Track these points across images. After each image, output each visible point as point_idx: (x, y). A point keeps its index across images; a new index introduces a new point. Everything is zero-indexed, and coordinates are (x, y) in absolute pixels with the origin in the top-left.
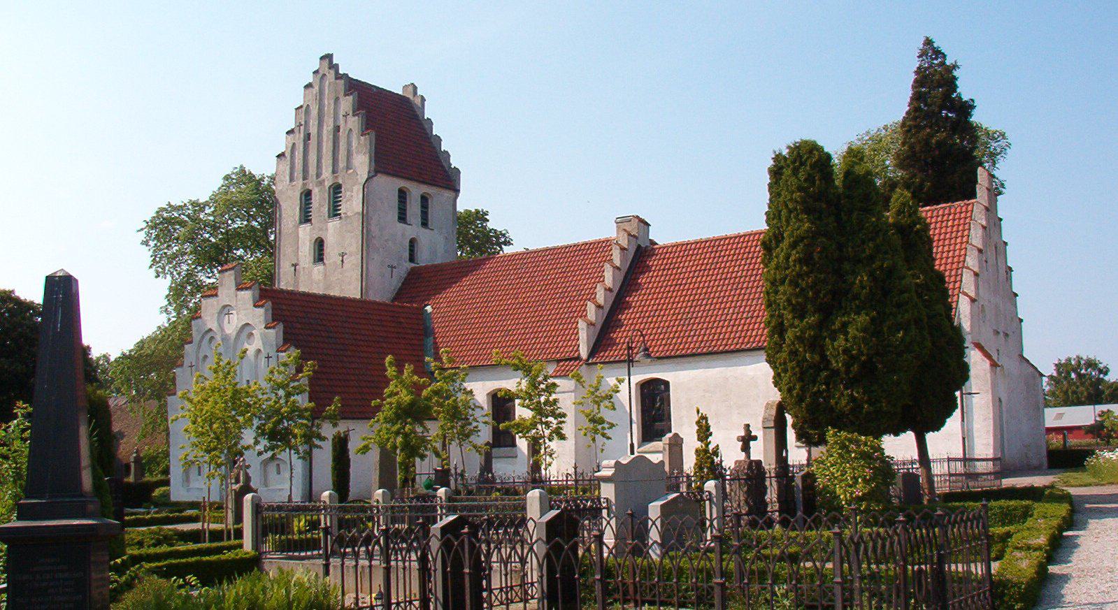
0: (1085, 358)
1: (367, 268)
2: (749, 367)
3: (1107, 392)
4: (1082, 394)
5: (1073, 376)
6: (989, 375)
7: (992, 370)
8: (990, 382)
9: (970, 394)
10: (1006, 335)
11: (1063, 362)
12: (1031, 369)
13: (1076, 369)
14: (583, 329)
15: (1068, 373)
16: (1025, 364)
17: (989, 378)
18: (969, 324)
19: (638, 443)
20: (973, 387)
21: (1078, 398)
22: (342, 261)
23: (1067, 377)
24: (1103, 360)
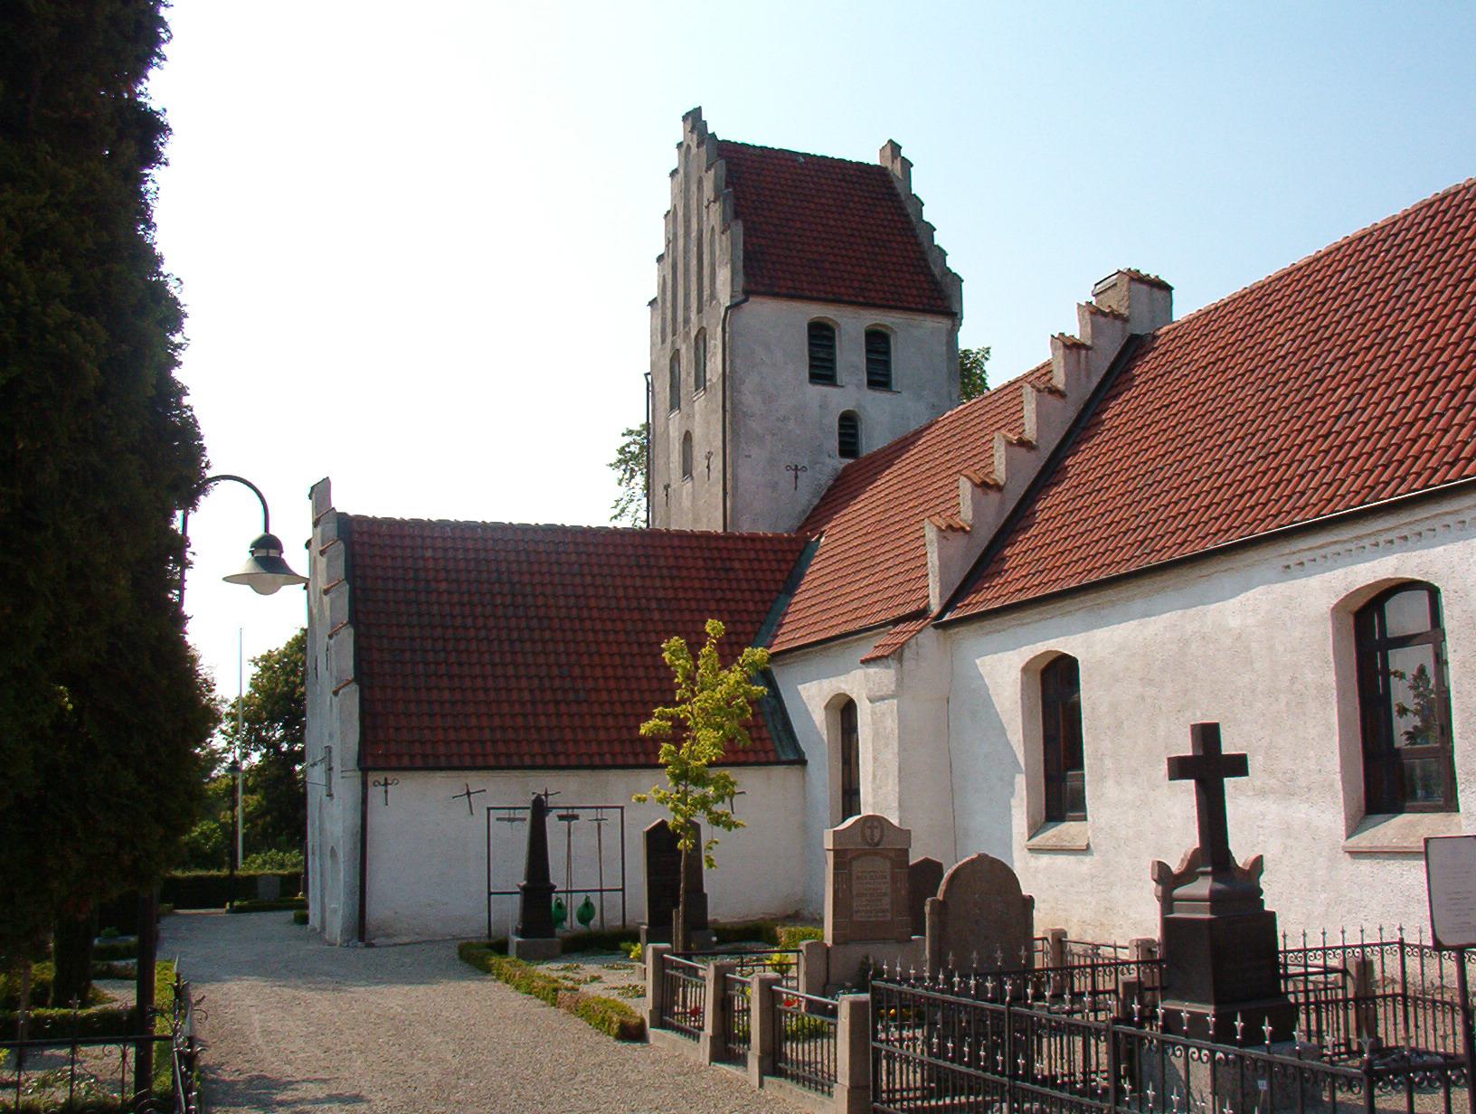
1: (734, 476)
2: (1233, 603)
14: (931, 541)
19: (1030, 816)
22: (708, 467)
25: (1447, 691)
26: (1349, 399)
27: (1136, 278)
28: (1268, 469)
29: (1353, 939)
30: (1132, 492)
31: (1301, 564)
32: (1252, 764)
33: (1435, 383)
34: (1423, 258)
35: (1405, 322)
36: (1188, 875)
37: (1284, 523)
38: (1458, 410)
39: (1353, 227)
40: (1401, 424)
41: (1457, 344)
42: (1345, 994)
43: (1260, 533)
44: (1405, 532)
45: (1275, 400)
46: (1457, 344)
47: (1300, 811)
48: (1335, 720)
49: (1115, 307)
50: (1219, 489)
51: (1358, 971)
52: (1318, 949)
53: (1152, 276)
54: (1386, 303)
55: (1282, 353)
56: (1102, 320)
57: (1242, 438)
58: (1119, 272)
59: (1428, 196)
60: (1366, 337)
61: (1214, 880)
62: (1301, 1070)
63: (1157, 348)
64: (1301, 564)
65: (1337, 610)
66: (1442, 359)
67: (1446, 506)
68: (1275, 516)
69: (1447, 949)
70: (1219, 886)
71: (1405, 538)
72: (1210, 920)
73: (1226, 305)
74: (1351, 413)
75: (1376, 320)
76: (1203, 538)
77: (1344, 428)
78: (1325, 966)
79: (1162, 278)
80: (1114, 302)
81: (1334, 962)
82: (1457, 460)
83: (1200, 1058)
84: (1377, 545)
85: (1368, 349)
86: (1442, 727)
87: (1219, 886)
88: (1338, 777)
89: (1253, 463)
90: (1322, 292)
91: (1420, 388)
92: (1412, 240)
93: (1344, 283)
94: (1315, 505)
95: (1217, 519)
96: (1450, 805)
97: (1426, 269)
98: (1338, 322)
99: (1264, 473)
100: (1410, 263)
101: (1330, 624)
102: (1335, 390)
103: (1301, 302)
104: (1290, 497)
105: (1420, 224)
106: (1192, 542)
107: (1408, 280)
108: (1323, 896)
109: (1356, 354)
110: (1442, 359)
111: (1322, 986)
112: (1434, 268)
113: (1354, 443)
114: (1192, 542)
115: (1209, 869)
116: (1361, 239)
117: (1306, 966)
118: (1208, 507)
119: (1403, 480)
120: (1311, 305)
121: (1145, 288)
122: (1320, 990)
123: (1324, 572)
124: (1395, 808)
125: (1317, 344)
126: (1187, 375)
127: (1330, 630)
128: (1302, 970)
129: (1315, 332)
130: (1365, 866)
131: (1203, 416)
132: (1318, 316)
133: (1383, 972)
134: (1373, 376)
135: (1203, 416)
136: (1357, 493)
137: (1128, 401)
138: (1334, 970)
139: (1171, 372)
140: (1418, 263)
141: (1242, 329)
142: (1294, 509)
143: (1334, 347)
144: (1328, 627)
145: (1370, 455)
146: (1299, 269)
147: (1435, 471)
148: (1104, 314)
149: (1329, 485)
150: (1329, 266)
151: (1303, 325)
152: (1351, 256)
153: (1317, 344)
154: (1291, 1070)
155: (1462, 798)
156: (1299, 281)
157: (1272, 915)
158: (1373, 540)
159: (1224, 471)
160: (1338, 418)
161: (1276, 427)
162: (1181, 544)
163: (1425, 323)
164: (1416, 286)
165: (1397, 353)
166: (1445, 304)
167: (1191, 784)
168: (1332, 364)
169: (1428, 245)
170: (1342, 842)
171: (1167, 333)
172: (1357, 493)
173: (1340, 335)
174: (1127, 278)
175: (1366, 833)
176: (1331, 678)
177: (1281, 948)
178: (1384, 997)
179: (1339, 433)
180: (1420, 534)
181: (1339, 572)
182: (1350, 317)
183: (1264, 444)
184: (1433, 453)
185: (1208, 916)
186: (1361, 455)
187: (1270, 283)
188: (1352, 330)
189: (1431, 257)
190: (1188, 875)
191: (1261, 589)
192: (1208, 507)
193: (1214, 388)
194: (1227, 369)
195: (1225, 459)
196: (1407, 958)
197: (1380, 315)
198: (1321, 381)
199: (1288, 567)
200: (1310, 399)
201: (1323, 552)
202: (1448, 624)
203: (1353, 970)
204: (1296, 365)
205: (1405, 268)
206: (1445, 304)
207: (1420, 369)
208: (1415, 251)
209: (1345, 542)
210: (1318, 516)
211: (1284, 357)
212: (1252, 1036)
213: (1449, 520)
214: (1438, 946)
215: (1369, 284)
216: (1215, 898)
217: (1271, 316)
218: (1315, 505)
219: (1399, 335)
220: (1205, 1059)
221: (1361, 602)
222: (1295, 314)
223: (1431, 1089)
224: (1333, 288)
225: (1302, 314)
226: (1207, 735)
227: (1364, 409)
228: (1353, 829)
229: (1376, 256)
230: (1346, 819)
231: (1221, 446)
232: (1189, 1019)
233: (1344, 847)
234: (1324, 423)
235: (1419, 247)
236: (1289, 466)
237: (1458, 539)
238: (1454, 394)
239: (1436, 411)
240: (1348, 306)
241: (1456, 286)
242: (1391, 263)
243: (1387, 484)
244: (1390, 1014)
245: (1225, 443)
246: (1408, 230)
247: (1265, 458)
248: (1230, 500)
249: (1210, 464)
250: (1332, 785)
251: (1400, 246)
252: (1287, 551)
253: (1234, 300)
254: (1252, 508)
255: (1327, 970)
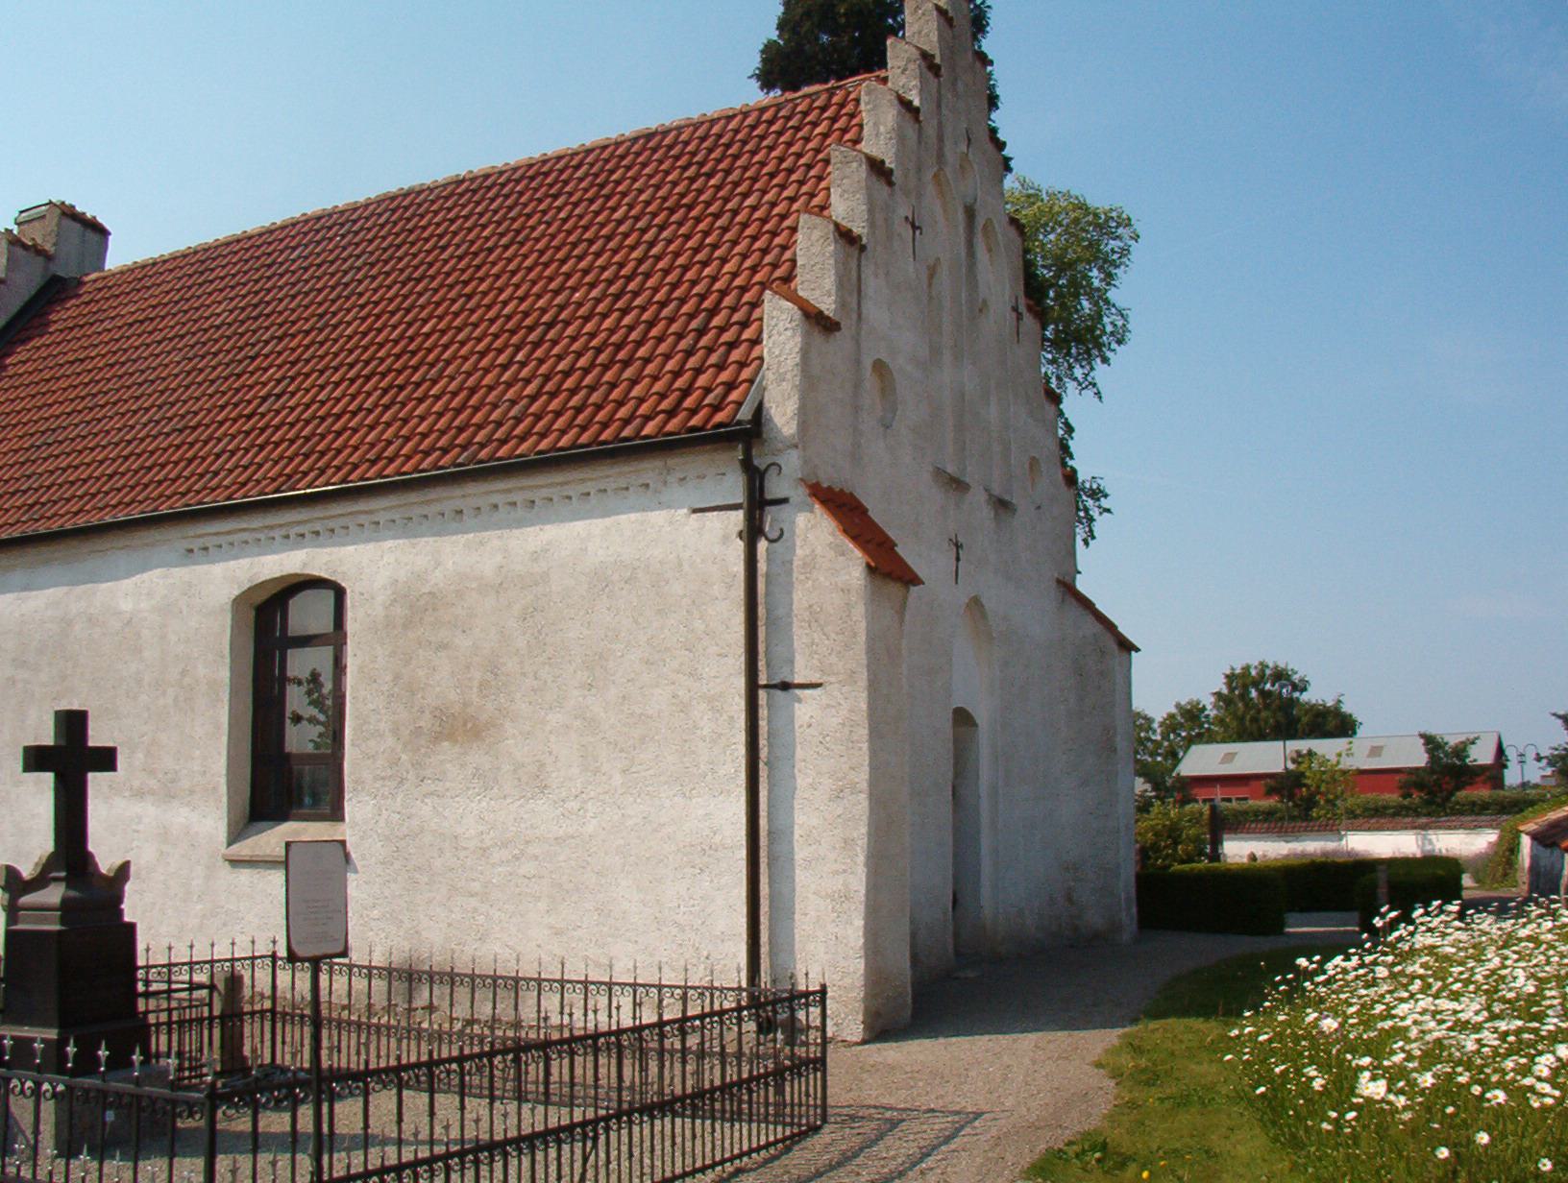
0: (1271, 665)
2: (127, 584)
3: (1305, 720)
4: (1266, 722)
5: (1254, 693)
6: (859, 611)
7: (874, 598)
8: (862, 638)
9: (786, 686)
10: (1002, 505)
11: (1238, 671)
12: (1092, 627)
13: (1256, 683)
15: (1245, 688)
16: (1074, 610)
17: (862, 627)
18: (792, 406)
20: (800, 662)
21: (1259, 729)
23: (1244, 696)
24: (1300, 669)
25: (343, 697)
26: (279, 381)
27: (69, 213)
28: (183, 443)
29: (222, 952)
30: (27, 449)
31: (206, 549)
32: (121, 761)
33: (368, 378)
34: (377, 249)
35: (349, 311)
36: (40, 881)
37: (192, 503)
38: (387, 408)
39: (312, 207)
40: (328, 415)
41: (396, 342)
42: (211, 1010)
43: (164, 510)
44: (318, 527)
45: (201, 371)
46: (396, 342)
47: (180, 816)
48: (225, 719)
49: (39, 241)
50: (127, 458)
51: (226, 985)
52: (183, 964)
53: (89, 215)
54: (333, 288)
55: (217, 323)
56: (20, 251)
57: (160, 407)
58: (50, 203)
59: (393, 189)
60: (307, 320)
61: (68, 887)
62: (139, 1097)
63: (81, 296)
64: (206, 549)
65: (239, 602)
66: (379, 355)
67: (362, 505)
68: (184, 495)
69: (303, 960)
70: (72, 893)
71: (317, 533)
72: (59, 932)
73: (165, 262)
74: (279, 396)
75: (320, 304)
76: (102, 509)
77: (269, 411)
78: (191, 982)
79: (100, 220)
80: (37, 235)
81: (201, 977)
82: (379, 458)
83: (22, 1091)
84: (287, 537)
85: (308, 333)
86: (335, 733)
87: (72, 893)
88: (223, 780)
89: (168, 435)
90: (269, 266)
91: (353, 381)
92: (369, 230)
93: (294, 261)
94: (227, 487)
95: (119, 490)
96: (336, 814)
97: (378, 261)
98: (281, 300)
99: (178, 447)
100: (363, 252)
101: (229, 617)
102: (266, 370)
103: (246, 273)
104: (202, 476)
105: (380, 215)
106: (89, 512)
107: (359, 269)
108: (199, 907)
109: (294, 336)
110: (379, 355)
111: (185, 1004)
112: (386, 262)
113: (278, 428)
114: (89, 512)
115: (63, 874)
116: (319, 218)
117: (170, 982)
118: (111, 476)
119: (322, 472)
120: (256, 277)
121: (77, 226)
122: (184, 1008)
123: (227, 560)
124: (282, 816)
125: (256, 319)
126: (109, 331)
127: (229, 622)
128: (164, 987)
129: (256, 306)
130: (245, 875)
131: (121, 377)
132: (262, 289)
133: (253, 986)
134: (308, 361)
135: (121, 377)
136: (274, 480)
137: (39, 348)
138: (201, 986)
139: (92, 324)
140: (372, 253)
141: (179, 290)
142: (205, 488)
143: (272, 325)
144: (227, 620)
145: (292, 442)
146: (250, 238)
147: (356, 467)
148: (24, 246)
149: (246, 468)
150: (282, 240)
151: (244, 297)
152: (306, 234)
153: (256, 319)
154: (126, 1100)
155: (348, 808)
156: (247, 250)
157: (132, 927)
158: (283, 532)
159: (135, 439)
160: (264, 399)
161: (198, 399)
162: (76, 514)
163: (369, 315)
164: (366, 277)
165: (336, 341)
166: (391, 300)
167: (48, 778)
168: (267, 342)
169: (384, 238)
170: (223, 849)
171: (95, 281)
172: (274, 480)
173: (281, 313)
174: (59, 211)
175: (249, 841)
176: (225, 674)
177: (141, 962)
178: (253, 1013)
179: (263, 415)
180: (332, 531)
181: (245, 562)
182: (294, 297)
183: (183, 417)
184: (356, 448)
185: (57, 927)
186: (282, 441)
187: (216, 247)
188: (294, 311)
189: (385, 250)
190: (40, 881)
191: (158, 572)
192: (111, 476)
193: (137, 348)
194: (155, 330)
195: (138, 427)
196: (278, 971)
197: (325, 300)
198: (253, 359)
199: (191, 551)
200: (239, 376)
201: (230, 538)
202: (351, 626)
203: (221, 986)
204: (229, 338)
205: (358, 257)
206: (391, 300)
207: (357, 361)
208: (371, 241)
209: (254, 530)
210: (245, 497)
211: (218, 328)
212: (86, 1063)
213: (363, 519)
214: (292, 958)
215: (320, 266)
216: (66, 906)
217: (212, 282)
218: (227, 487)
219: (340, 323)
220: (28, 1092)
221: (263, 596)
222: (238, 284)
223: (278, 1106)
224: (282, 264)
225: (245, 285)
226: (73, 723)
227: (293, 394)
228: (235, 836)
229: (331, 239)
230: (229, 825)
231: (135, 412)
232: (12, 1047)
233: (223, 856)
234: (250, 402)
235: (375, 237)
236: (206, 443)
237: (368, 540)
238: (386, 391)
239: (365, 406)
240: (294, 285)
241: (404, 284)
242: (344, 248)
243: (305, 474)
244: (258, 1032)
245: (140, 409)
246: (367, 219)
247: (181, 431)
248: (136, 472)
249: (120, 430)
250: (215, 789)
251: (357, 233)
252: (191, 533)
253: (175, 259)
254: (160, 483)
255: (193, 987)
